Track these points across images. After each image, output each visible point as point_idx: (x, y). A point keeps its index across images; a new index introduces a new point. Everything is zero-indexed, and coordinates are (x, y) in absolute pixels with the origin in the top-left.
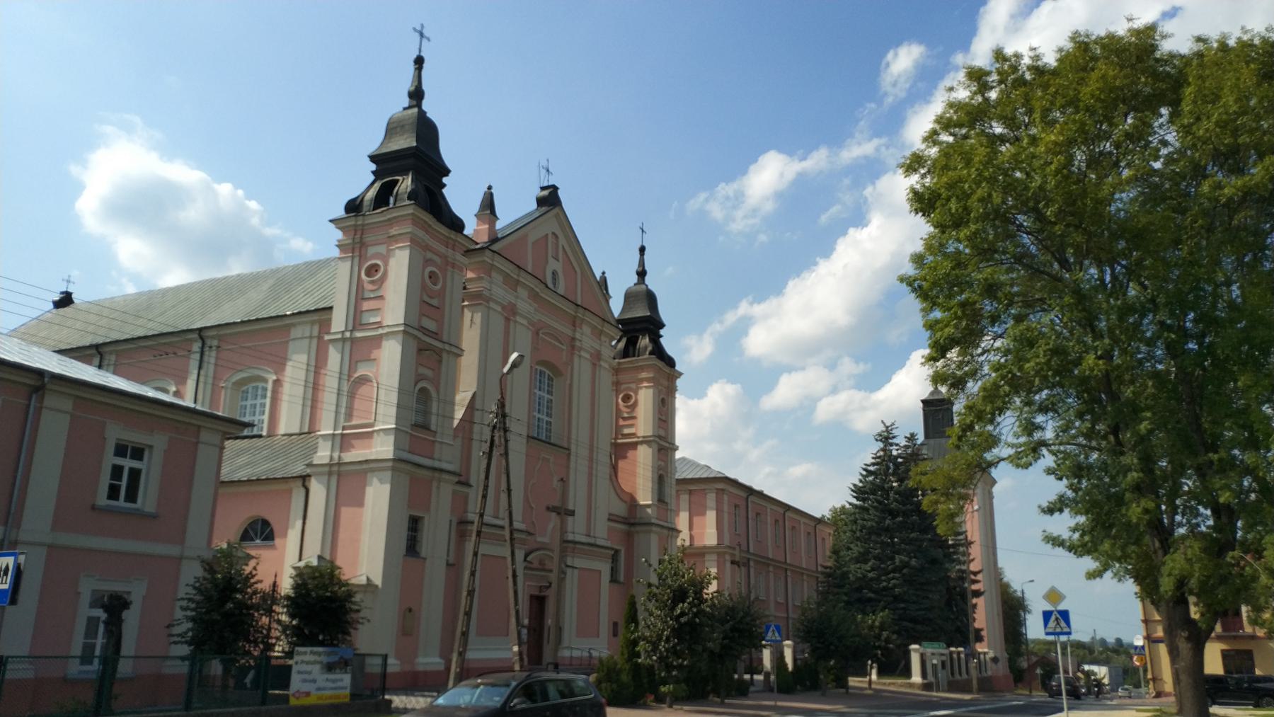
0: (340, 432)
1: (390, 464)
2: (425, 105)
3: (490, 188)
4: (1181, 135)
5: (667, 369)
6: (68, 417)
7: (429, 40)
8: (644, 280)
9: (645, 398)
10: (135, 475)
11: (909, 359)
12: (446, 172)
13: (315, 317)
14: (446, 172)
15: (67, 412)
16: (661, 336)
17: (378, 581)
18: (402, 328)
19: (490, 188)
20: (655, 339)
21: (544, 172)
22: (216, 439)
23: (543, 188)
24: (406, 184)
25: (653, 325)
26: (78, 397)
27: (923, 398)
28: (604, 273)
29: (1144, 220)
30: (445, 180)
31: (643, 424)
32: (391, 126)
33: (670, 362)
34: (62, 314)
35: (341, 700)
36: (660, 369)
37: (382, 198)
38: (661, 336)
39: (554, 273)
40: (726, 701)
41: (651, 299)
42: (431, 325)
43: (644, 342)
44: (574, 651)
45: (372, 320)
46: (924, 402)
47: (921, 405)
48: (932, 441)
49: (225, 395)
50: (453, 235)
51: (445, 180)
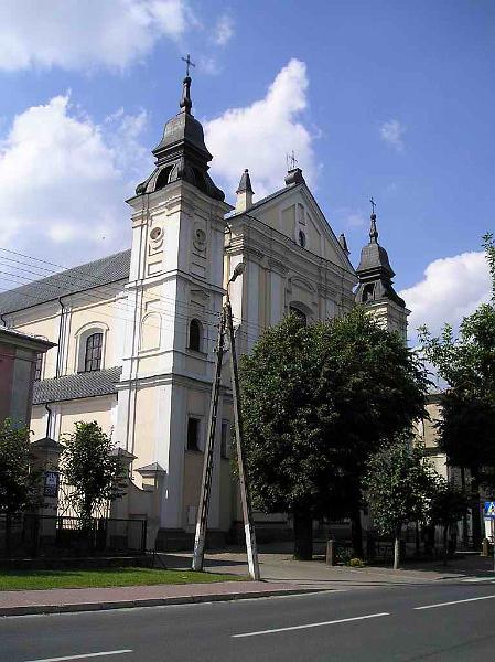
2: (193, 112)
3: (247, 171)
5: (398, 308)
7: (183, 59)
11: (444, 259)
12: (210, 158)
14: (210, 157)
17: (165, 466)
18: (176, 273)
19: (247, 171)
20: (388, 285)
21: (290, 160)
22: (28, 355)
24: (179, 164)
25: (386, 274)
29: (369, 497)
33: (401, 303)
34: (51, 268)
35: (124, 575)
37: (162, 181)
39: (301, 234)
40: (448, 563)
42: (200, 272)
43: (379, 286)
50: (215, 203)
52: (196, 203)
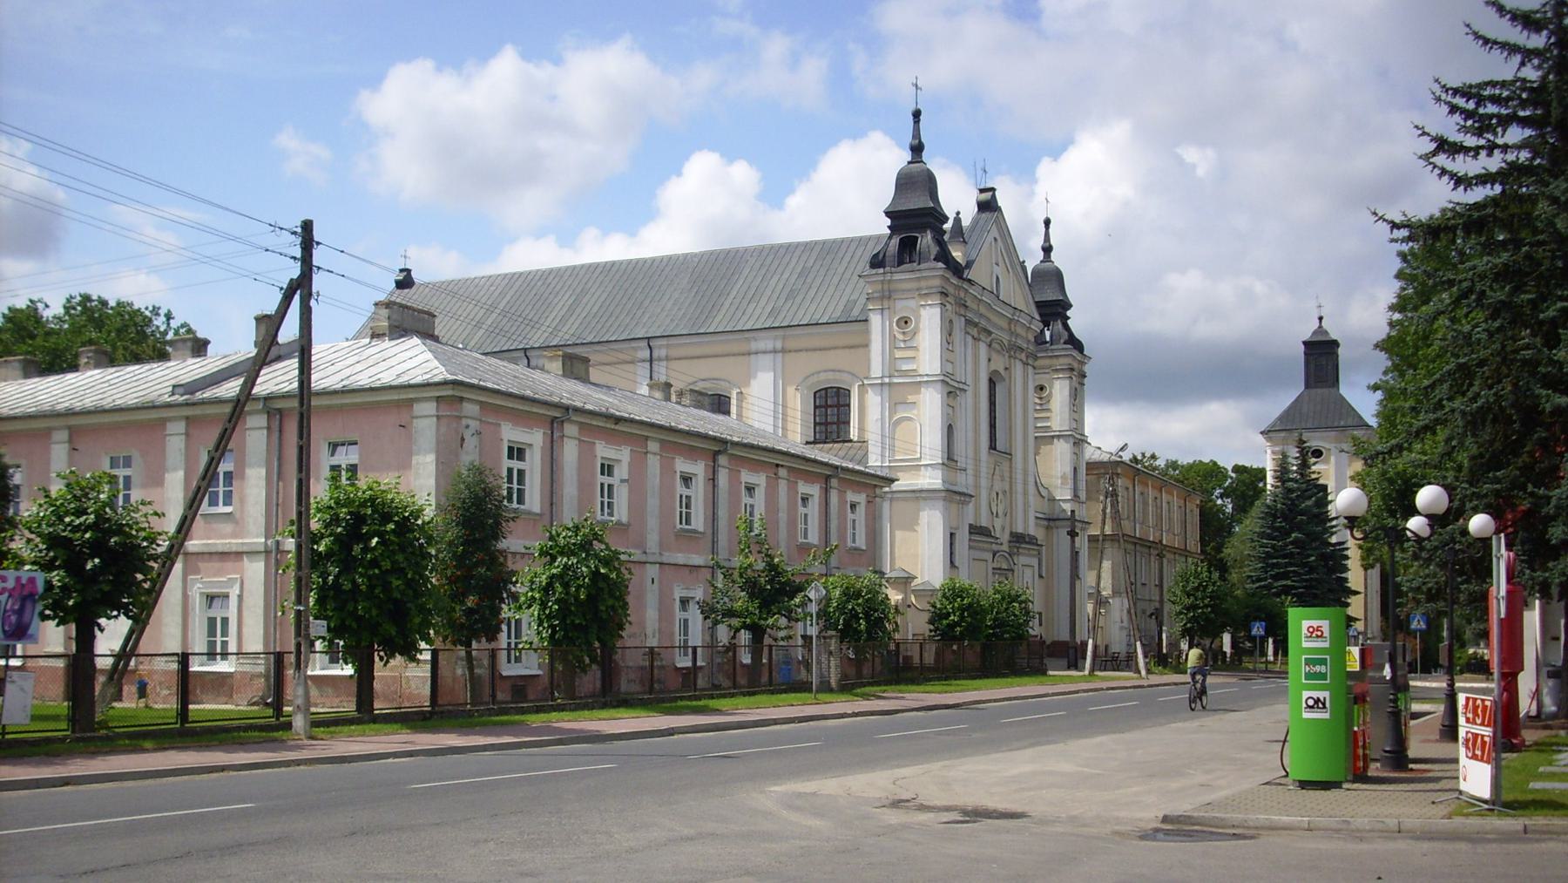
0: (887, 464)
1: (943, 494)
4: (1526, 547)
5: (1075, 353)
6: (435, 419)
8: (1050, 257)
9: (1060, 391)
10: (521, 473)
13: (780, 333)
15: (432, 416)
16: (1069, 318)
23: (982, 191)
26: (582, 423)
27: (1304, 339)
28: (958, 213)
30: (1069, 313)
31: (1058, 418)
32: (902, 181)
36: (948, 279)
38: (1069, 318)
41: (1057, 277)
44: (506, 652)
45: (905, 367)
46: (1305, 343)
47: (1303, 347)
48: (1313, 391)
49: (1499, 612)
51: (1069, 313)
52: (951, 290)
